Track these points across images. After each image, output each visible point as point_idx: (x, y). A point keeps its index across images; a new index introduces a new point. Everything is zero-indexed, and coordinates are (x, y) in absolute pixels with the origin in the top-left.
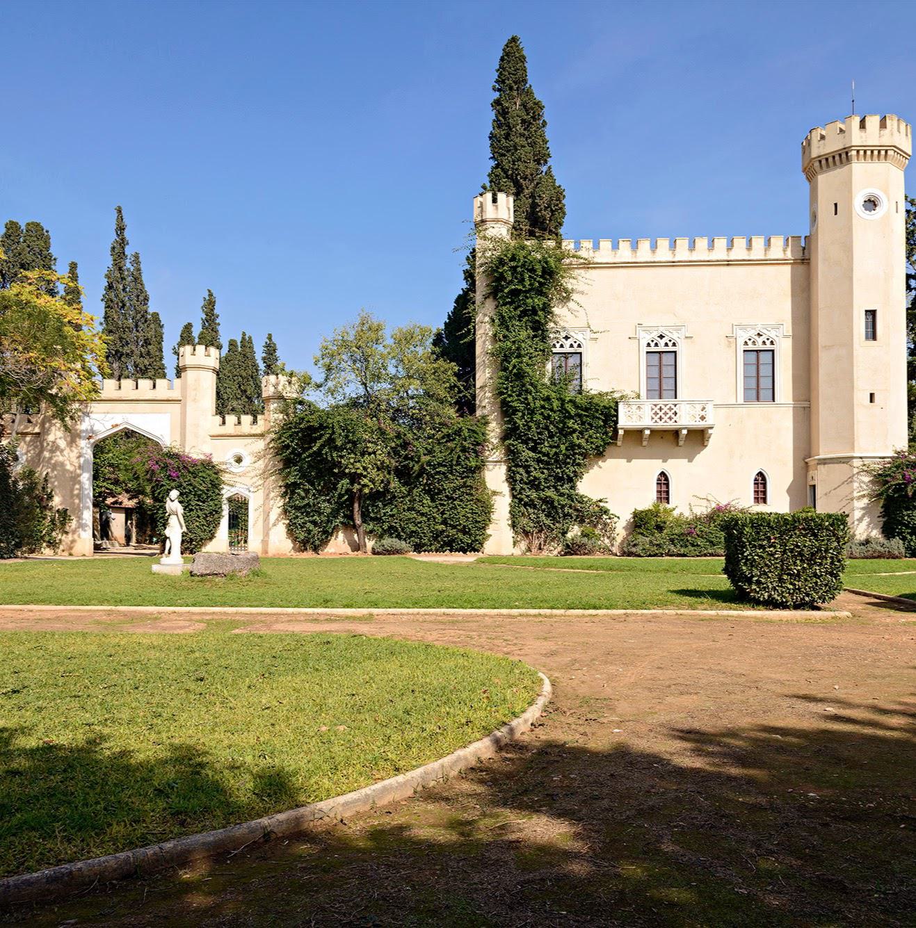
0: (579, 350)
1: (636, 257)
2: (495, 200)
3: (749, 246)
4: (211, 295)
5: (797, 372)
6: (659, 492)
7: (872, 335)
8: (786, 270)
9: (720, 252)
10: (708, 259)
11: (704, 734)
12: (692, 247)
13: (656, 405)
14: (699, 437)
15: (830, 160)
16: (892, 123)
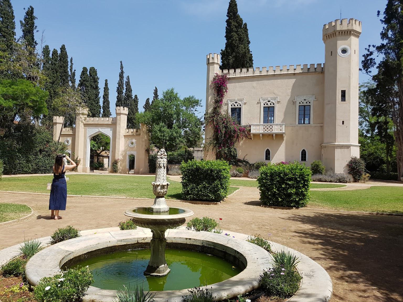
0: (309, 104)
4: (156, 89)
11: (354, 283)
15: (343, 33)
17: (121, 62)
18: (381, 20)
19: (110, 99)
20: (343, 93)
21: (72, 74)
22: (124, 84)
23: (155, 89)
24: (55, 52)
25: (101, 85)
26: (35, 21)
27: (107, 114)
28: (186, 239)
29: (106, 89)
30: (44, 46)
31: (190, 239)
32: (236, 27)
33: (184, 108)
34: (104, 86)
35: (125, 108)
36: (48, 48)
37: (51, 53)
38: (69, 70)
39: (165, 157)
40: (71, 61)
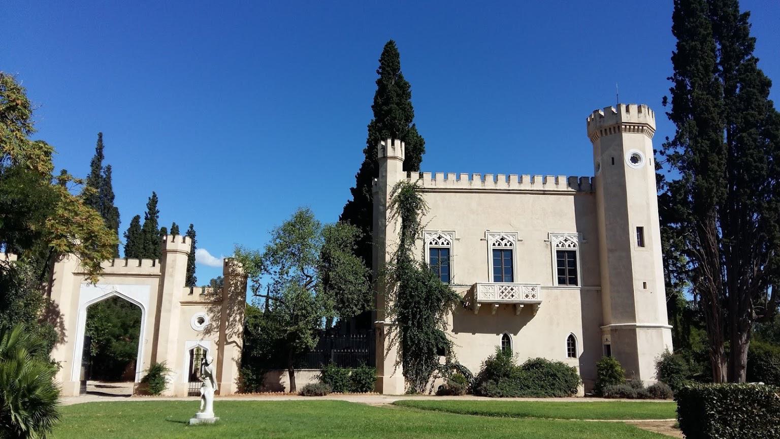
1: (484, 185)
2: (393, 144)
3: (533, 182)
4: (154, 196)
5: (590, 264)
6: (569, 350)
7: (641, 243)
8: (571, 199)
9: (538, 186)
10: (530, 189)
12: (520, 181)
13: (509, 287)
14: (530, 310)
16: (644, 110)
17: (100, 135)
18: (667, 113)
20: (640, 230)
23: (151, 196)
32: (398, 95)
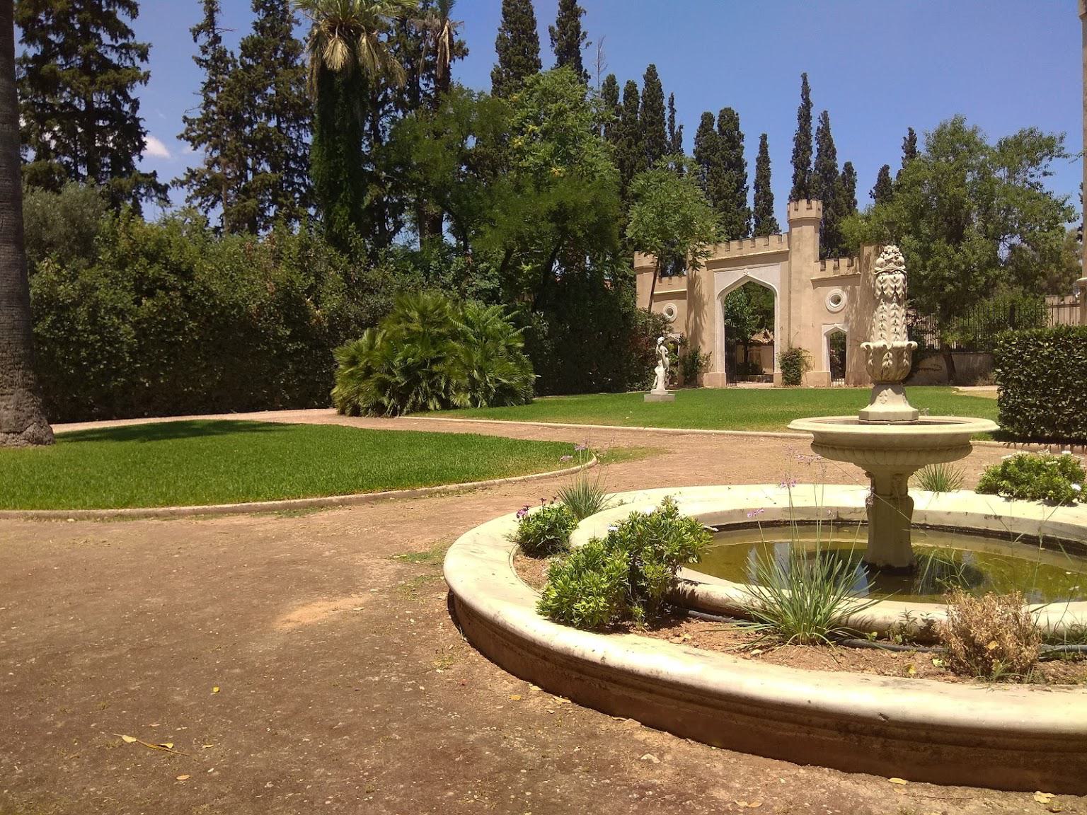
19: (773, 189)
21: (673, 139)
22: (813, 139)
24: (631, 90)
25: (750, 155)
26: (582, 20)
27: (766, 226)
28: (986, 517)
29: (763, 160)
30: (603, 78)
31: (1000, 517)
33: (1001, 174)
34: (757, 154)
35: (814, 203)
36: (615, 83)
37: (621, 94)
38: (667, 130)
39: (899, 268)
40: (671, 104)
